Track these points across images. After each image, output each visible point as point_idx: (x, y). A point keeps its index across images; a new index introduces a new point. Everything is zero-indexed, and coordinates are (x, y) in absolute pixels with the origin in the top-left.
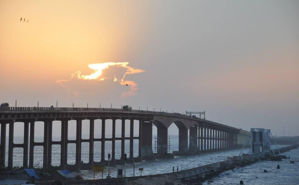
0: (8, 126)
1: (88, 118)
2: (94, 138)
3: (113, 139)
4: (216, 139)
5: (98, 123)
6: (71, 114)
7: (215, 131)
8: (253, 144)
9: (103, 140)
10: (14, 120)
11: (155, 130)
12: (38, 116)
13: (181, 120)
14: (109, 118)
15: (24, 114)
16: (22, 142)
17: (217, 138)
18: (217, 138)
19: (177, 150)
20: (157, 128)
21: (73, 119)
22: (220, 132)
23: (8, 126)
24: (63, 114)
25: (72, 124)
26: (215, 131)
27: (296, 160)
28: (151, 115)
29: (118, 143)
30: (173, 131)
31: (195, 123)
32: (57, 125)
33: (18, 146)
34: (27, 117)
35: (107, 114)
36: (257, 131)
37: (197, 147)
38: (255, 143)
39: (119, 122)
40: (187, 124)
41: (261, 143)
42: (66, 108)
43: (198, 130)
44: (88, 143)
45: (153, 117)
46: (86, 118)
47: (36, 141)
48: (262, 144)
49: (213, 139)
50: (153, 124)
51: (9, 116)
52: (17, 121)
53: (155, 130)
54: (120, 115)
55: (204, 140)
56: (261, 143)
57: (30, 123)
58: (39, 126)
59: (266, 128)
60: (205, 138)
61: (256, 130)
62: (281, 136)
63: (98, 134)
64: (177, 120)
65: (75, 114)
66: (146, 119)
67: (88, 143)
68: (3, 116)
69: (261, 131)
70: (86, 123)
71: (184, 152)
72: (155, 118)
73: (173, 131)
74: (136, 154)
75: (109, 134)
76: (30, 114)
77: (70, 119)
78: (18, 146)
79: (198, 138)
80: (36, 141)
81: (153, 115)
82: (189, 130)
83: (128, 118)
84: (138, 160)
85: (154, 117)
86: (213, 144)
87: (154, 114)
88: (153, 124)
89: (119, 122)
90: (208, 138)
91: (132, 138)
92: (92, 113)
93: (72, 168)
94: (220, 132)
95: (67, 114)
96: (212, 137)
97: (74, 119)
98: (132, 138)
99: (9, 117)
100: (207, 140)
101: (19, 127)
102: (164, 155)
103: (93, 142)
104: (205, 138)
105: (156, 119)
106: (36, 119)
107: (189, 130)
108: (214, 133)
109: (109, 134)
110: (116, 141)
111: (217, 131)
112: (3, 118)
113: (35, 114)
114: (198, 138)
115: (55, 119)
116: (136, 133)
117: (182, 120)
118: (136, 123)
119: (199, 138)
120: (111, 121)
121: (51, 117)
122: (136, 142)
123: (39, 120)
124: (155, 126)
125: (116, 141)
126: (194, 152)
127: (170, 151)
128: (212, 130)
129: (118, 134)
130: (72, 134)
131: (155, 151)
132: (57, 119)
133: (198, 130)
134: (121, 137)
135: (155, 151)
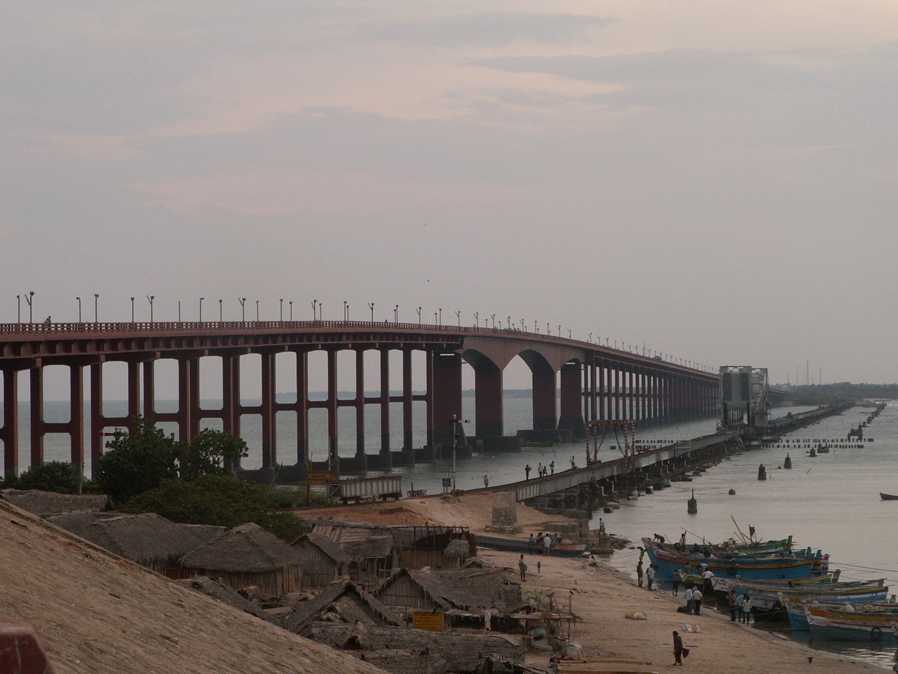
0: (87, 371)
1: (291, 349)
2: (307, 400)
3: (384, 399)
4: (630, 395)
5: (317, 359)
6: (247, 338)
7: (627, 374)
8: (725, 405)
9: (332, 403)
10: (103, 357)
11: (468, 375)
12: (42, 348)
13: (538, 352)
14: (345, 347)
15: (127, 342)
16: (66, 418)
17: (641, 393)
18: (641, 393)
19: (529, 425)
20: (531, 374)
21: (252, 352)
22: (640, 376)
23: (87, 371)
24: (225, 338)
25: (250, 365)
26: (627, 374)
27: (834, 444)
28: (458, 336)
29: (372, 412)
30: (517, 376)
31: (573, 355)
32: (211, 368)
33: (396, 399)
34: (75, 352)
35: (368, 335)
36: (736, 370)
37: (554, 419)
38: (729, 403)
39: (372, 357)
40: (553, 358)
41: (744, 403)
42: (168, 324)
43: (583, 372)
44: (378, 406)
45: (462, 342)
46: (320, 347)
47: (48, 418)
48: (748, 404)
49: (624, 395)
50: (463, 361)
51: (23, 349)
52: (110, 358)
53: (468, 375)
54: (400, 339)
55: (598, 399)
56: (744, 403)
57: (142, 365)
58: (166, 372)
59: (756, 364)
60: (601, 394)
61: (731, 369)
62: (800, 384)
63: (317, 387)
64: (527, 347)
65: (256, 338)
66: (444, 347)
67: (378, 406)
68: (6, 350)
69: (745, 371)
70: (286, 361)
71: (543, 434)
72: (468, 344)
73: (517, 376)
74: (420, 441)
75: (346, 387)
76: (141, 341)
77: (244, 352)
78: (396, 399)
79: (584, 394)
80: (48, 418)
81: (462, 337)
82: (558, 374)
83: (397, 347)
84: (422, 456)
85: (466, 341)
86: (625, 410)
87: (464, 334)
88: (463, 361)
89: (396, 356)
90: (609, 395)
91: (407, 398)
92: (301, 336)
93: (289, 475)
94: (640, 376)
95: (236, 338)
96: (621, 391)
97: (254, 351)
98: (407, 398)
99: (90, 351)
100: (606, 400)
101: (57, 378)
102: (493, 441)
103: (307, 409)
104: (601, 394)
105: (472, 347)
106: (158, 354)
107: (558, 374)
108: (628, 380)
109: (346, 387)
110: (367, 407)
111: (634, 375)
112: (7, 355)
113: (155, 341)
114: (584, 394)
115: (249, 350)
116: (420, 385)
117: (534, 347)
118: (419, 358)
119: (586, 394)
120: (292, 356)
121: (196, 347)
122: (420, 409)
123: (165, 355)
124: (468, 364)
125: (367, 407)
126: (574, 430)
127: (510, 428)
128: (621, 373)
129: (372, 387)
130: (250, 391)
131: (470, 430)
132: (212, 353)
133: (583, 372)
134: (294, 400)
135: (470, 430)
